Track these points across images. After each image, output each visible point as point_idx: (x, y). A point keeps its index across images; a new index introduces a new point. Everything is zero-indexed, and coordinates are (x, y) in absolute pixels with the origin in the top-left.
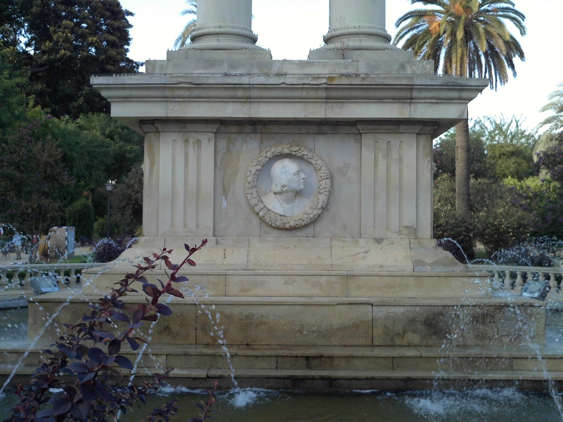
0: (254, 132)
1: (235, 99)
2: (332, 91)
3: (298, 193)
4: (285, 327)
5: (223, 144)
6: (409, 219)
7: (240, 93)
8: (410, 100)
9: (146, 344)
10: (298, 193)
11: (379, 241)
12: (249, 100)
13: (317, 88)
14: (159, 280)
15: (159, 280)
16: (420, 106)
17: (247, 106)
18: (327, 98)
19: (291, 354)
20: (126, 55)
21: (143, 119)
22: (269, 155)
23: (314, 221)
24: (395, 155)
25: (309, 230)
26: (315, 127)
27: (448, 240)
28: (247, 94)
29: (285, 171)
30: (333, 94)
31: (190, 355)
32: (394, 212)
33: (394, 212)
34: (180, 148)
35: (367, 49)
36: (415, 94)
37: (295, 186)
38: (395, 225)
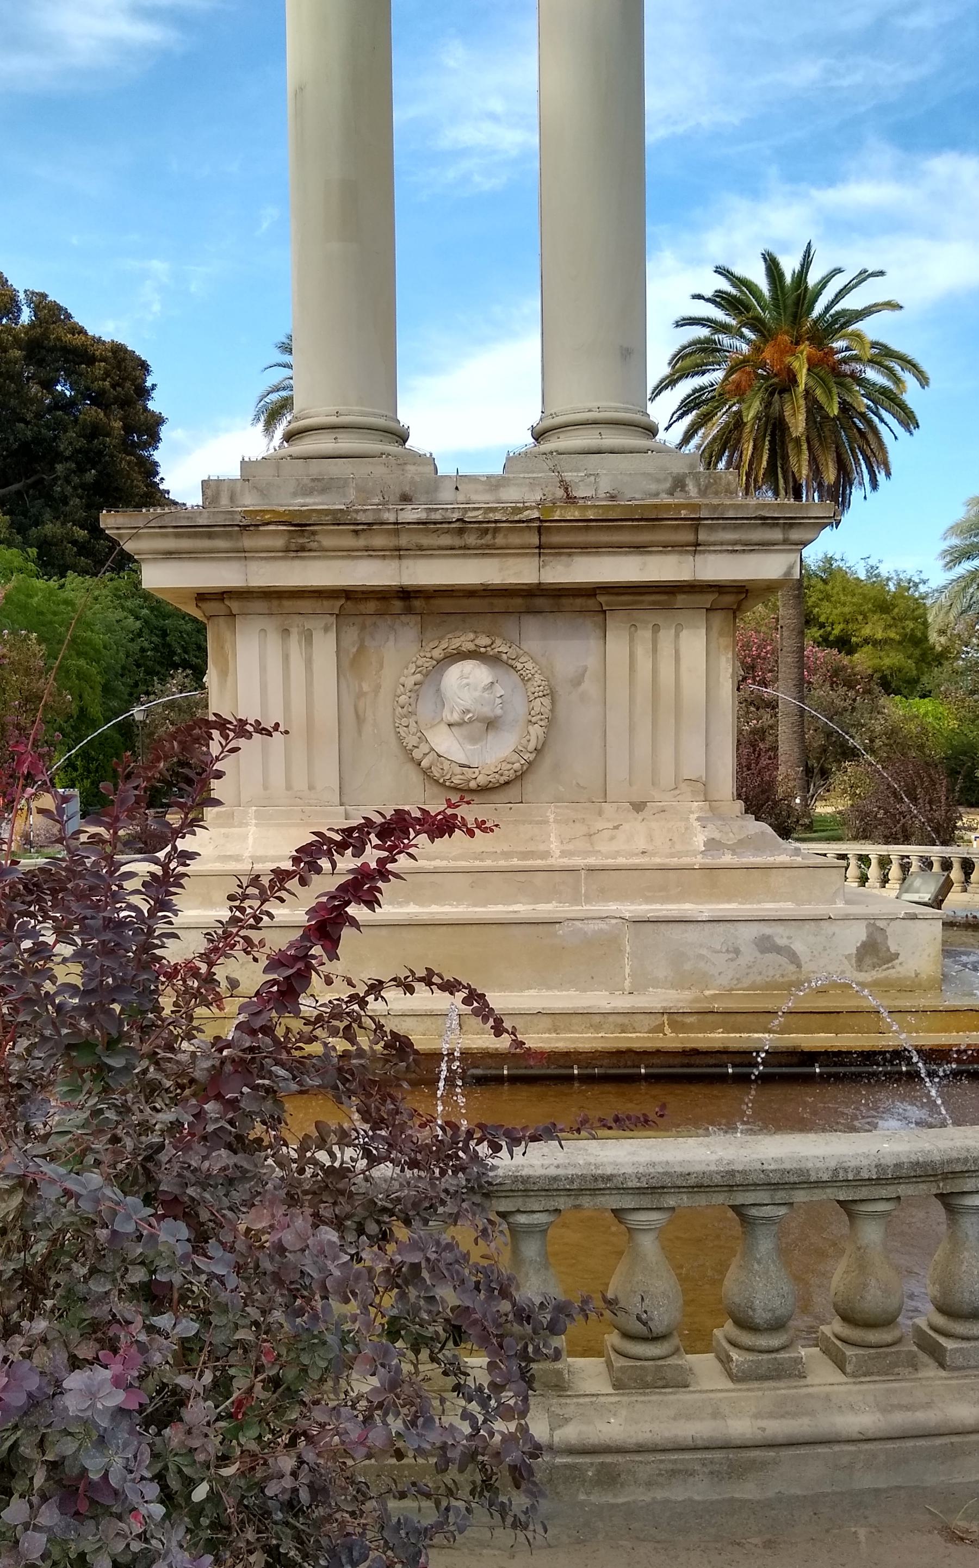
0: (409, 611)
2: (545, 533)
3: (491, 724)
5: (351, 635)
6: (694, 766)
10: (491, 724)
11: (638, 807)
12: (399, 553)
16: (711, 558)
17: (394, 564)
23: (520, 776)
25: (513, 792)
26: (519, 601)
29: (467, 683)
30: (556, 539)
34: (273, 640)
36: (500, 540)
37: (486, 711)
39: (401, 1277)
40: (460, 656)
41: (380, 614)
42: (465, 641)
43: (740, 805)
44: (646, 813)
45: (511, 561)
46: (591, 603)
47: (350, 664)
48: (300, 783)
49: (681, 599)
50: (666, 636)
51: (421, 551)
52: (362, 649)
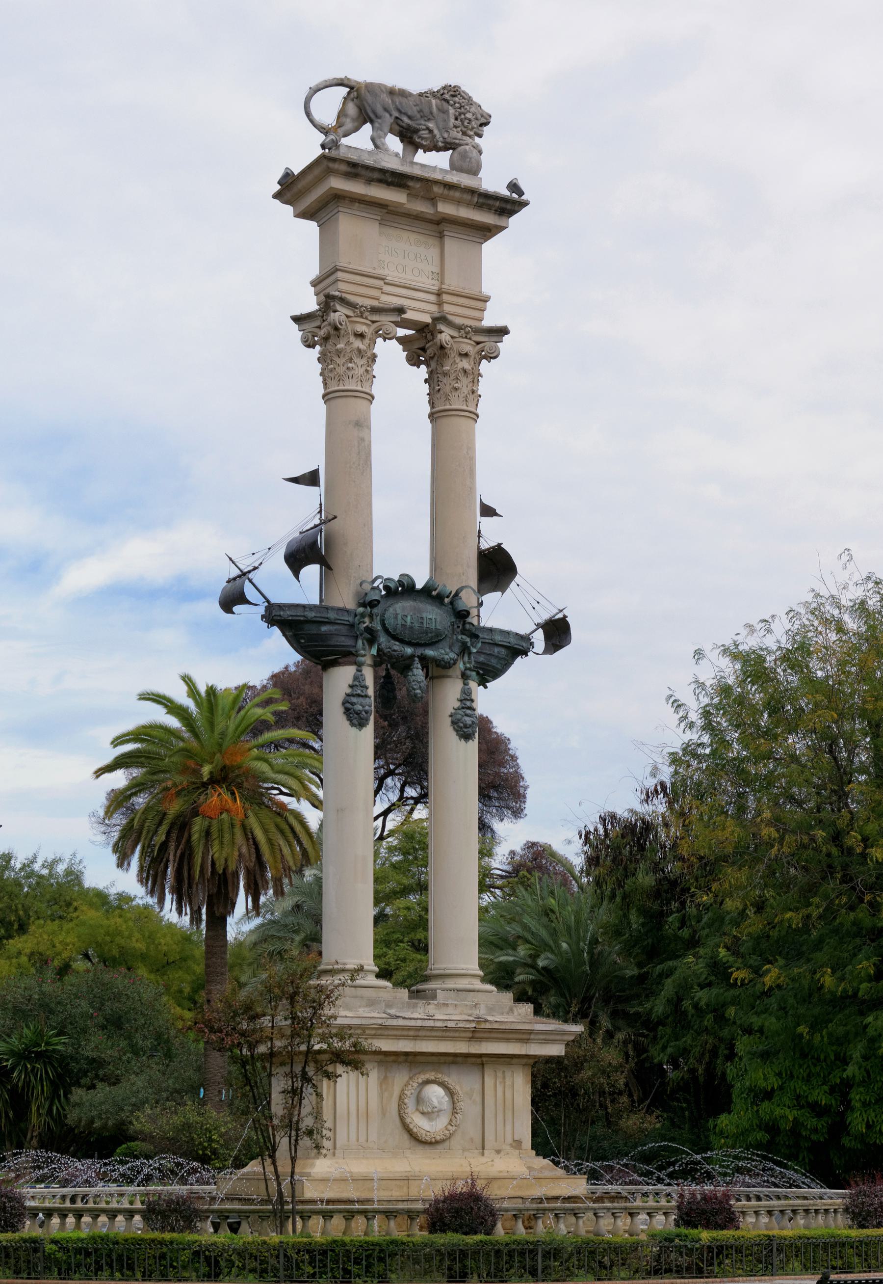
0: (406, 1061)
1: (406, 1037)
4: (647, 817)
7: (411, 1033)
8: (527, 1041)
9: (754, 1220)
11: (498, 1152)
13: (465, 1030)
14: (256, 605)
15: (256, 605)
16: (533, 1045)
17: (413, 1042)
18: (530, 1033)
19: (430, 1018)
20: (297, 665)
21: (339, 193)
22: (420, 1081)
23: (431, 1143)
24: (508, 1082)
27: (15, 1229)
28: (417, 1033)
30: (478, 1035)
31: (158, 827)
32: (509, 1128)
33: (509, 1128)
35: (478, 991)
36: (532, 1037)
38: (509, 1140)
39: (798, 1077)
40: (428, 1082)
41: (394, 1062)
42: (431, 1076)
43: (534, 1152)
44: (502, 1153)
45: (458, 1043)
46: (479, 1061)
47: (384, 1082)
48: (362, 1139)
49: (515, 1061)
50: (508, 1074)
51: (487, 1039)
52: (386, 1077)
